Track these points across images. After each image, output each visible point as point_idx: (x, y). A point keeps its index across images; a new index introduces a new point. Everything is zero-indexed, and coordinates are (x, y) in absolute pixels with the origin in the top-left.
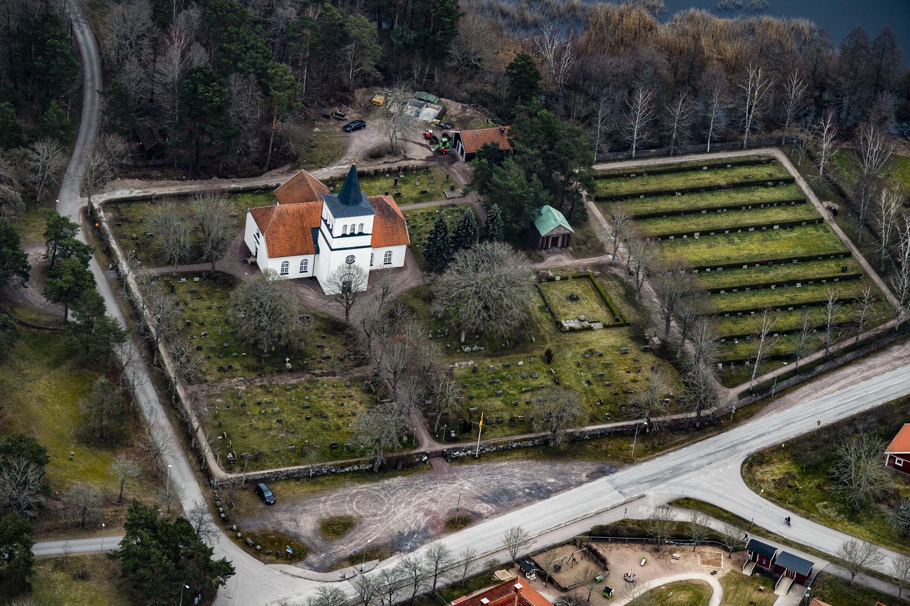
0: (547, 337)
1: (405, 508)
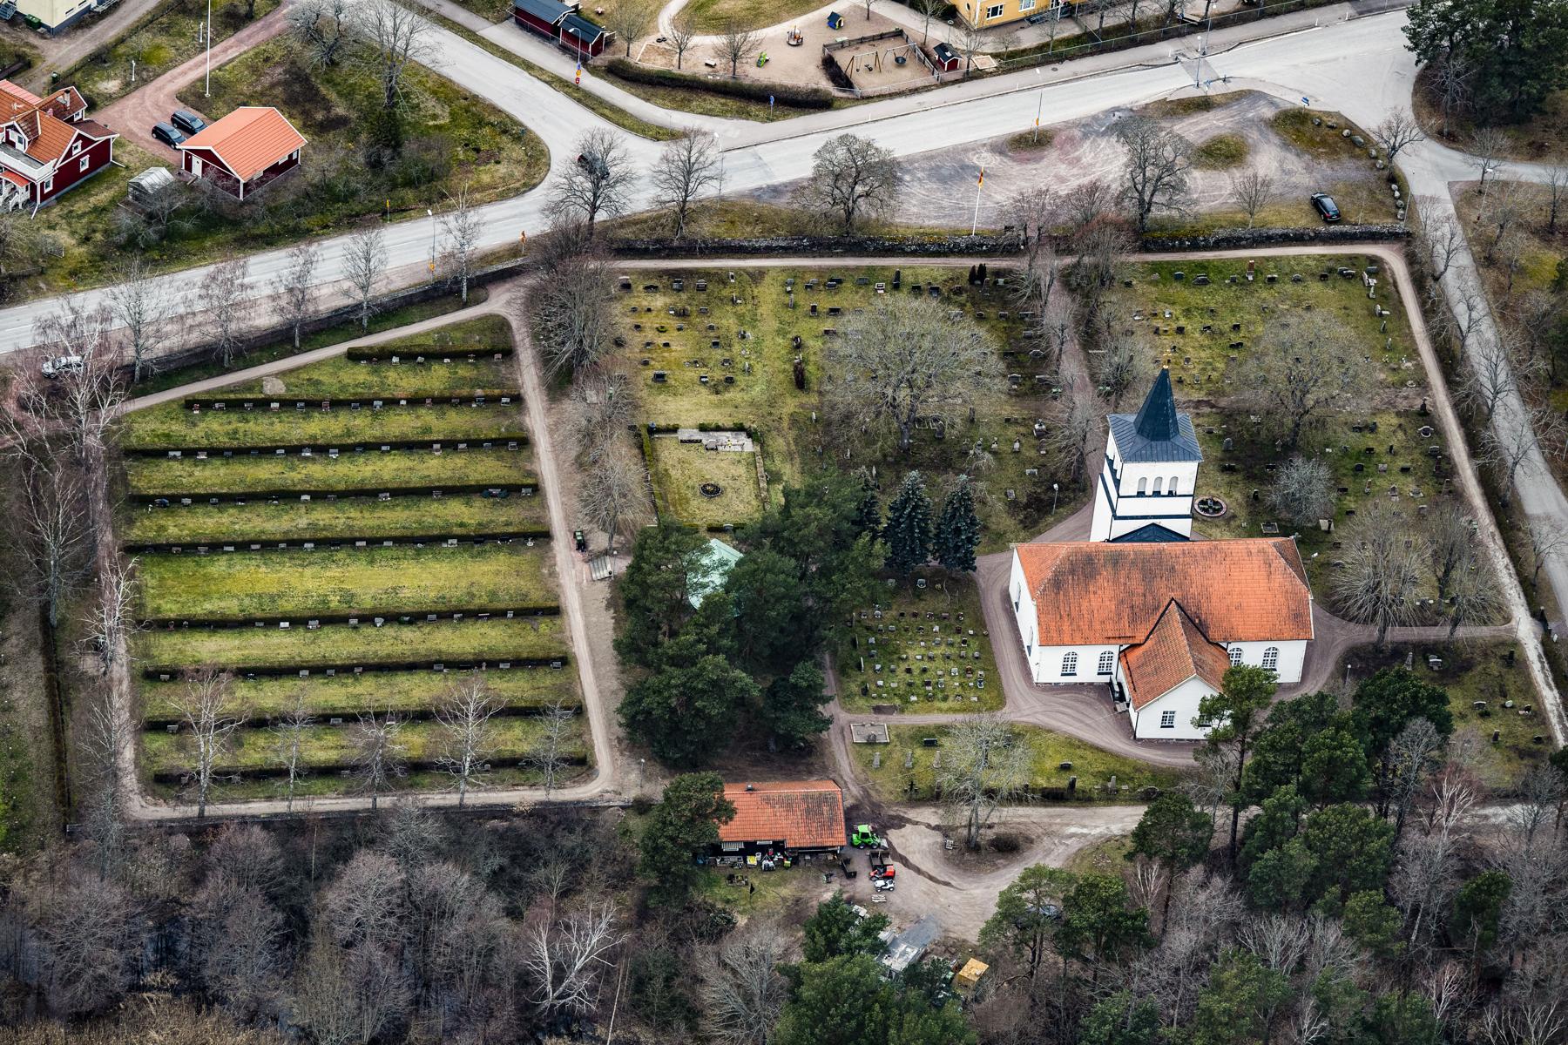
0: (785, 424)
1: (1109, 172)
